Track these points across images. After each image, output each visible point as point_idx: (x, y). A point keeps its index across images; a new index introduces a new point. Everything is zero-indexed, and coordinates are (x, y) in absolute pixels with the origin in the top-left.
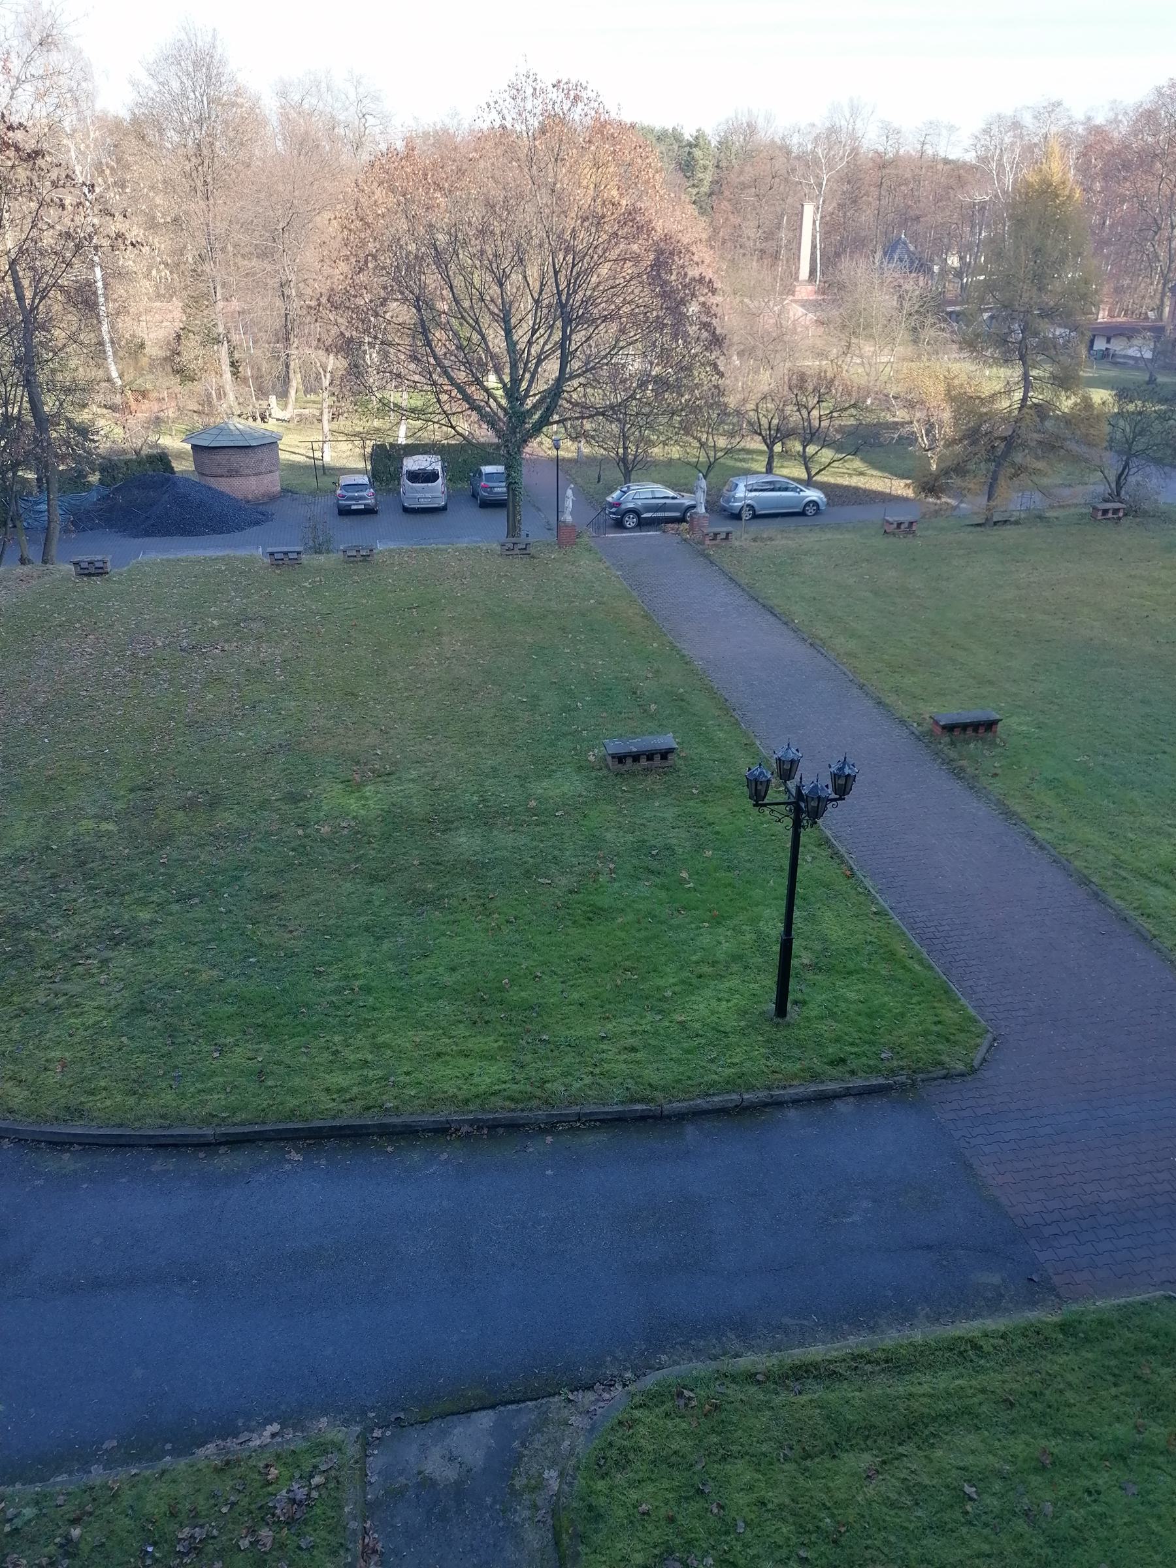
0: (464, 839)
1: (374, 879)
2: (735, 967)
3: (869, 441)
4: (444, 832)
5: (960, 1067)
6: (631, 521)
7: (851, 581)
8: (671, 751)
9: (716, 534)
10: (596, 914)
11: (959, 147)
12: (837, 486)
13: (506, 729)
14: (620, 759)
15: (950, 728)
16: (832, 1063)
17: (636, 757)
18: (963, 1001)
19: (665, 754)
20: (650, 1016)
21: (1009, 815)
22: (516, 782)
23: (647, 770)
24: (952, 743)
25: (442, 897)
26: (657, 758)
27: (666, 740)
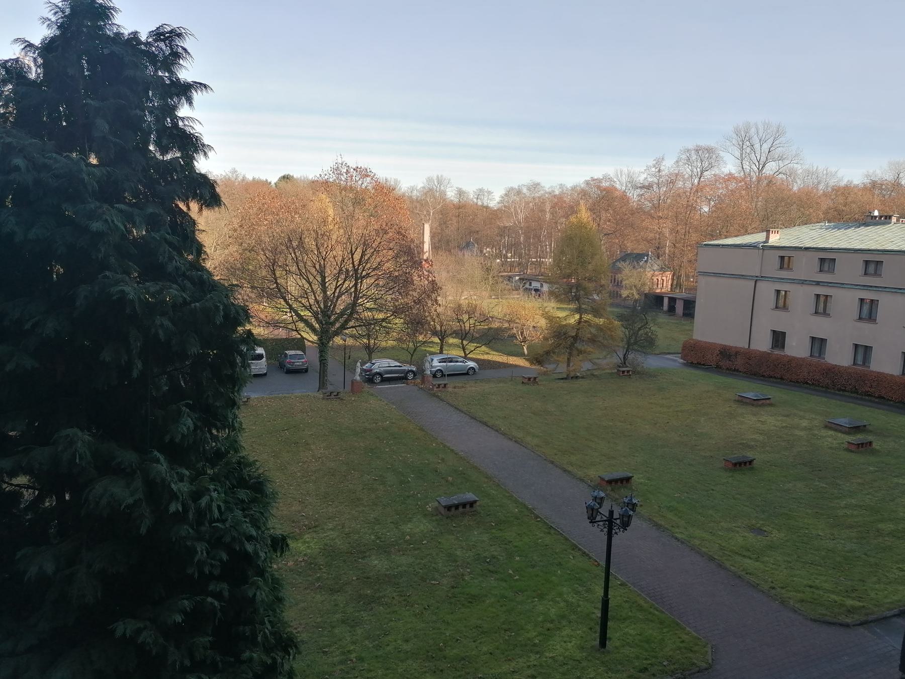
0: (376, 562)
1: (333, 591)
2: (564, 623)
3: (493, 337)
4: (363, 558)
5: (704, 665)
6: (378, 379)
7: (519, 408)
8: (475, 502)
9: (439, 385)
10: (473, 599)
11: (494, 202)
12: (484, 360)
13: (373, 496)
14: (449, 508)
15: (610, 482)
16: (641, 671)
17: (457, 507)
18: (688, 629)
19: (472, 504)
20: (533, 657)
21: (658, 526)
22: (392, 526)
23: (463, 514)
24: (612, 490)
25: (379, 598)
26: (468, 506)
27: (470, 496)
